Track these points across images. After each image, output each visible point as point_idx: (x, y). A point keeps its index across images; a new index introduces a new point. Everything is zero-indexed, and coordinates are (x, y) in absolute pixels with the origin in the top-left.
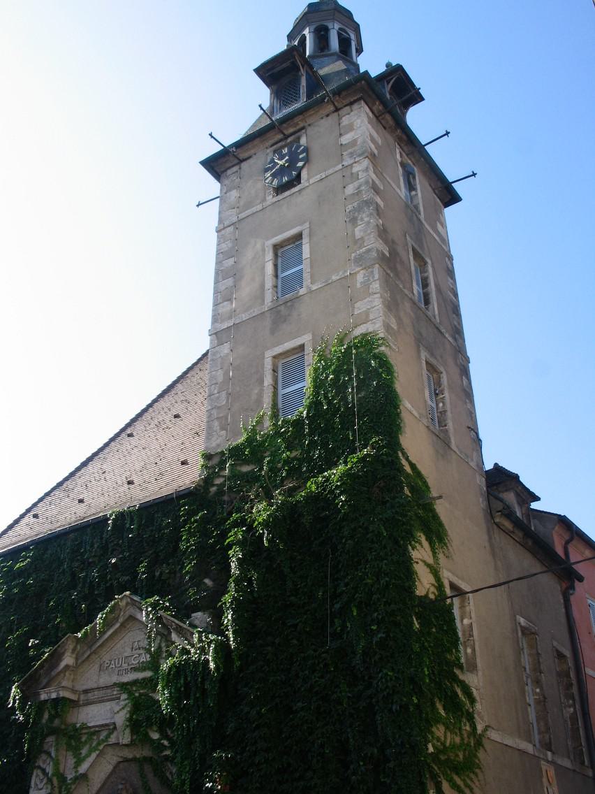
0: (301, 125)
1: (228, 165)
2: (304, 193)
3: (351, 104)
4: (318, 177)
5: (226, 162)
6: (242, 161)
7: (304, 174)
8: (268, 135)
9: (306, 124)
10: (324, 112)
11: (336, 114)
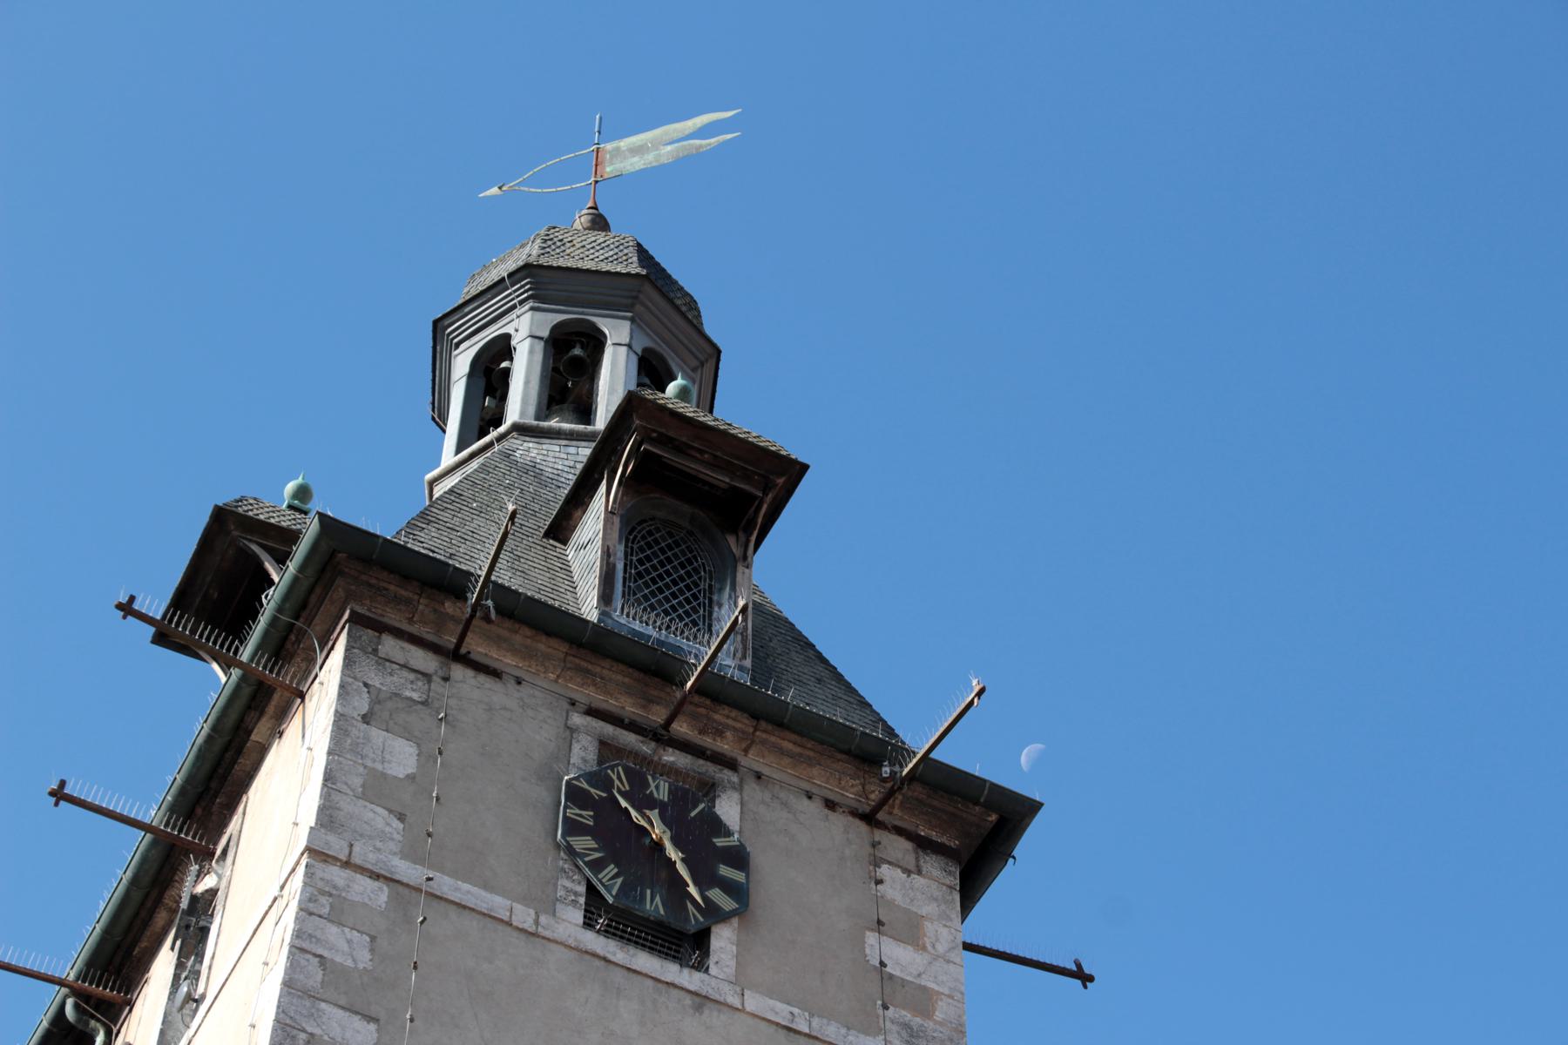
0: (725, 746)
1: (393, 618)
2: (711, 1016)
3: (923, 845)
4: (780, 1011)
5: (397, 600)
6: (457, 655)
7: (723, 940)
8: (604, 668)
9: (744, 761)
10: (822, 779)
11: (863, 827)
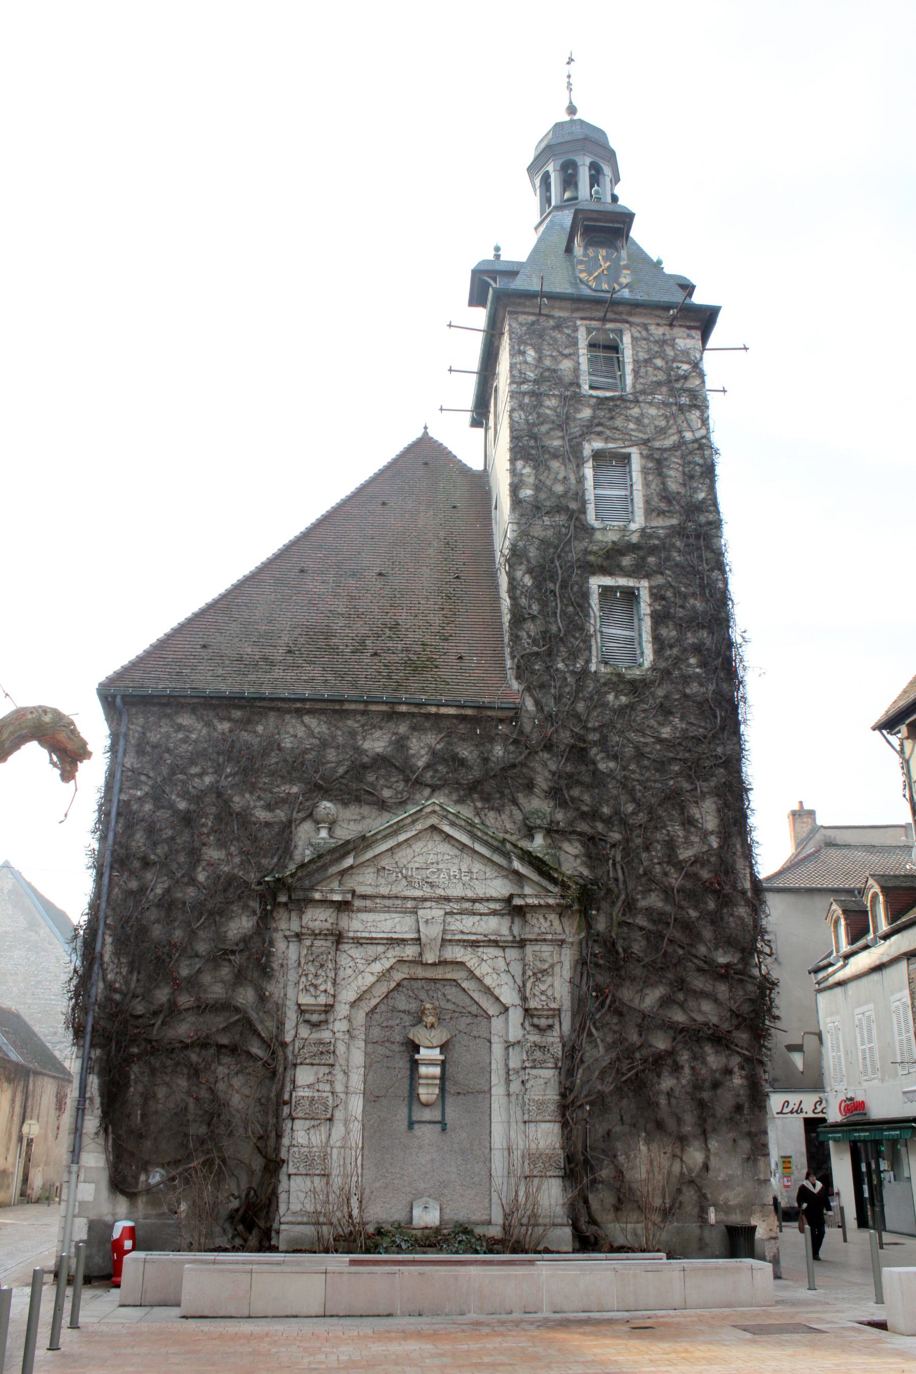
5: (519, 304)
